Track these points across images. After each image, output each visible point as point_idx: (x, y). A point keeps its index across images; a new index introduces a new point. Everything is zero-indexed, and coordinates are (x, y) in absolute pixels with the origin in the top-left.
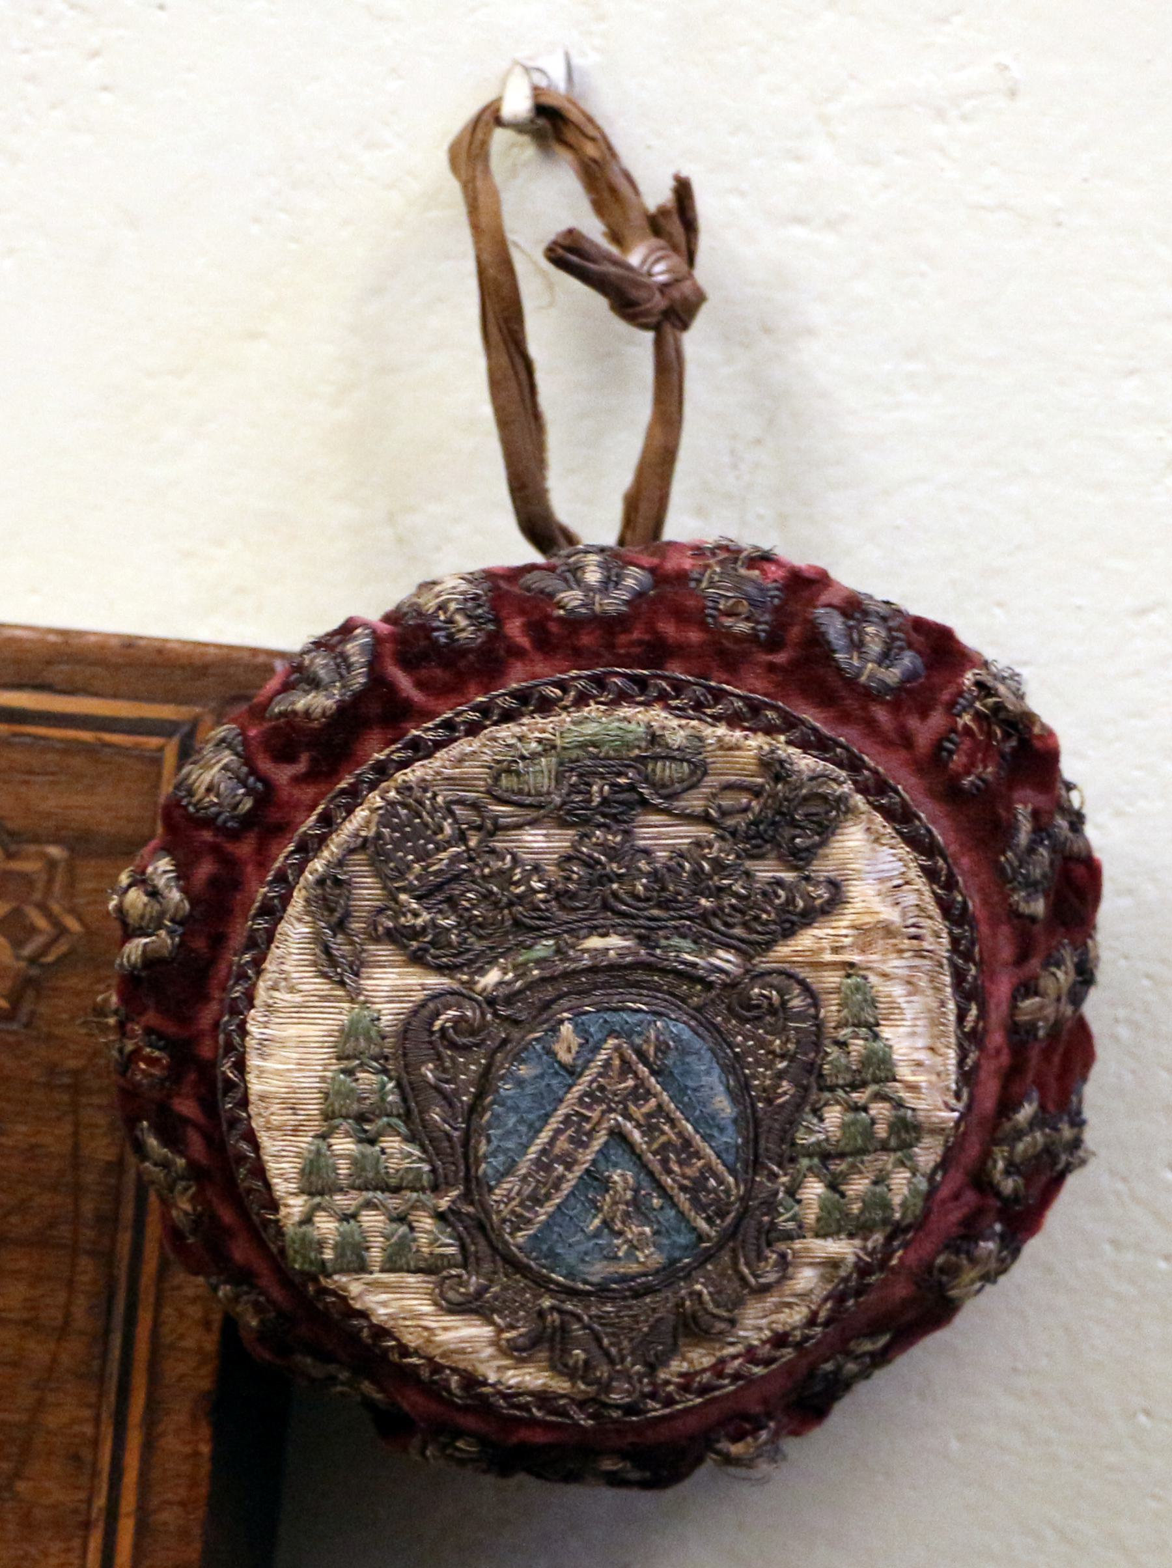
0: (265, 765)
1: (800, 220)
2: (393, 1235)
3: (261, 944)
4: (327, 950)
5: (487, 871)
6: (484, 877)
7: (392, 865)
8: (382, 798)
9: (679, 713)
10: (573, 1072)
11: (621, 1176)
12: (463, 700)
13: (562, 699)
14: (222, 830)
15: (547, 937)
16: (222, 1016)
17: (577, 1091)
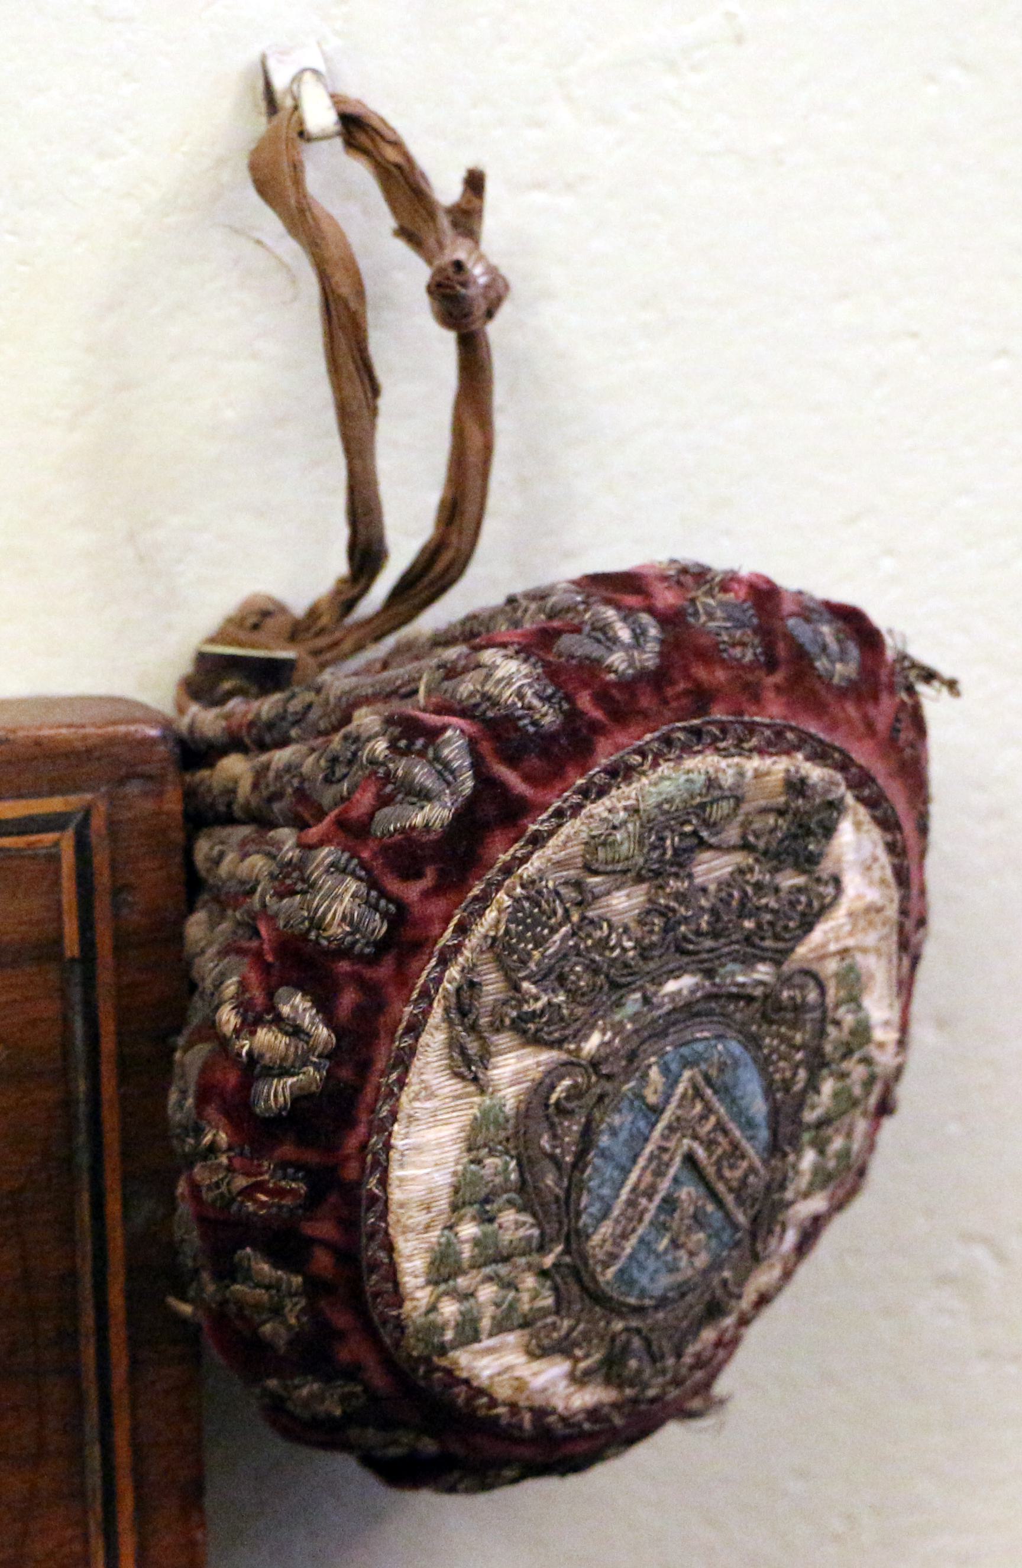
0: (394, 885)
1: (539, 185)
2: (503, 1302)
3: (404, 1061)
4: (463, 1051)
5: (590, 942)
6: (587, 948)
7: (515, 957)
8: (508, 895)
9: (726, 754)
10: (657, 1111)
11: (688, 1192)
12: (564, 785)
13: (642, 765)
14: (361, 958)
15: (634, 991)
16: (370, 1136)
17: (660, 1126)
